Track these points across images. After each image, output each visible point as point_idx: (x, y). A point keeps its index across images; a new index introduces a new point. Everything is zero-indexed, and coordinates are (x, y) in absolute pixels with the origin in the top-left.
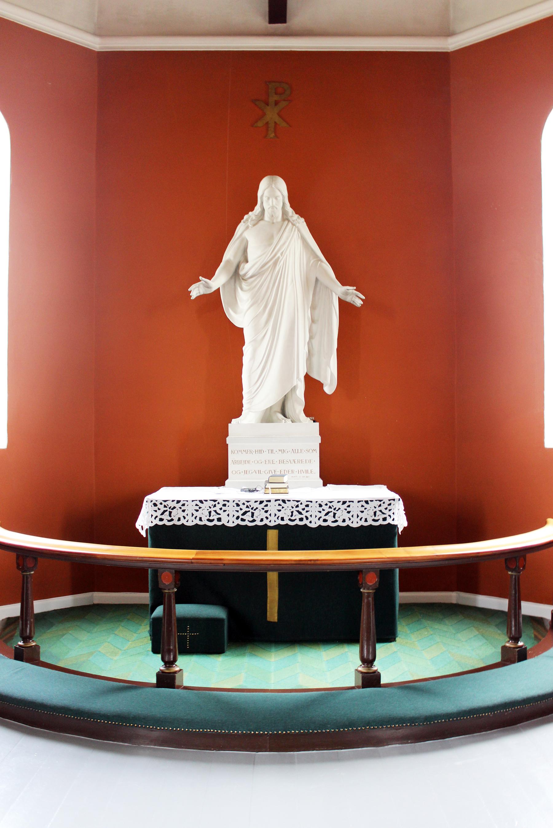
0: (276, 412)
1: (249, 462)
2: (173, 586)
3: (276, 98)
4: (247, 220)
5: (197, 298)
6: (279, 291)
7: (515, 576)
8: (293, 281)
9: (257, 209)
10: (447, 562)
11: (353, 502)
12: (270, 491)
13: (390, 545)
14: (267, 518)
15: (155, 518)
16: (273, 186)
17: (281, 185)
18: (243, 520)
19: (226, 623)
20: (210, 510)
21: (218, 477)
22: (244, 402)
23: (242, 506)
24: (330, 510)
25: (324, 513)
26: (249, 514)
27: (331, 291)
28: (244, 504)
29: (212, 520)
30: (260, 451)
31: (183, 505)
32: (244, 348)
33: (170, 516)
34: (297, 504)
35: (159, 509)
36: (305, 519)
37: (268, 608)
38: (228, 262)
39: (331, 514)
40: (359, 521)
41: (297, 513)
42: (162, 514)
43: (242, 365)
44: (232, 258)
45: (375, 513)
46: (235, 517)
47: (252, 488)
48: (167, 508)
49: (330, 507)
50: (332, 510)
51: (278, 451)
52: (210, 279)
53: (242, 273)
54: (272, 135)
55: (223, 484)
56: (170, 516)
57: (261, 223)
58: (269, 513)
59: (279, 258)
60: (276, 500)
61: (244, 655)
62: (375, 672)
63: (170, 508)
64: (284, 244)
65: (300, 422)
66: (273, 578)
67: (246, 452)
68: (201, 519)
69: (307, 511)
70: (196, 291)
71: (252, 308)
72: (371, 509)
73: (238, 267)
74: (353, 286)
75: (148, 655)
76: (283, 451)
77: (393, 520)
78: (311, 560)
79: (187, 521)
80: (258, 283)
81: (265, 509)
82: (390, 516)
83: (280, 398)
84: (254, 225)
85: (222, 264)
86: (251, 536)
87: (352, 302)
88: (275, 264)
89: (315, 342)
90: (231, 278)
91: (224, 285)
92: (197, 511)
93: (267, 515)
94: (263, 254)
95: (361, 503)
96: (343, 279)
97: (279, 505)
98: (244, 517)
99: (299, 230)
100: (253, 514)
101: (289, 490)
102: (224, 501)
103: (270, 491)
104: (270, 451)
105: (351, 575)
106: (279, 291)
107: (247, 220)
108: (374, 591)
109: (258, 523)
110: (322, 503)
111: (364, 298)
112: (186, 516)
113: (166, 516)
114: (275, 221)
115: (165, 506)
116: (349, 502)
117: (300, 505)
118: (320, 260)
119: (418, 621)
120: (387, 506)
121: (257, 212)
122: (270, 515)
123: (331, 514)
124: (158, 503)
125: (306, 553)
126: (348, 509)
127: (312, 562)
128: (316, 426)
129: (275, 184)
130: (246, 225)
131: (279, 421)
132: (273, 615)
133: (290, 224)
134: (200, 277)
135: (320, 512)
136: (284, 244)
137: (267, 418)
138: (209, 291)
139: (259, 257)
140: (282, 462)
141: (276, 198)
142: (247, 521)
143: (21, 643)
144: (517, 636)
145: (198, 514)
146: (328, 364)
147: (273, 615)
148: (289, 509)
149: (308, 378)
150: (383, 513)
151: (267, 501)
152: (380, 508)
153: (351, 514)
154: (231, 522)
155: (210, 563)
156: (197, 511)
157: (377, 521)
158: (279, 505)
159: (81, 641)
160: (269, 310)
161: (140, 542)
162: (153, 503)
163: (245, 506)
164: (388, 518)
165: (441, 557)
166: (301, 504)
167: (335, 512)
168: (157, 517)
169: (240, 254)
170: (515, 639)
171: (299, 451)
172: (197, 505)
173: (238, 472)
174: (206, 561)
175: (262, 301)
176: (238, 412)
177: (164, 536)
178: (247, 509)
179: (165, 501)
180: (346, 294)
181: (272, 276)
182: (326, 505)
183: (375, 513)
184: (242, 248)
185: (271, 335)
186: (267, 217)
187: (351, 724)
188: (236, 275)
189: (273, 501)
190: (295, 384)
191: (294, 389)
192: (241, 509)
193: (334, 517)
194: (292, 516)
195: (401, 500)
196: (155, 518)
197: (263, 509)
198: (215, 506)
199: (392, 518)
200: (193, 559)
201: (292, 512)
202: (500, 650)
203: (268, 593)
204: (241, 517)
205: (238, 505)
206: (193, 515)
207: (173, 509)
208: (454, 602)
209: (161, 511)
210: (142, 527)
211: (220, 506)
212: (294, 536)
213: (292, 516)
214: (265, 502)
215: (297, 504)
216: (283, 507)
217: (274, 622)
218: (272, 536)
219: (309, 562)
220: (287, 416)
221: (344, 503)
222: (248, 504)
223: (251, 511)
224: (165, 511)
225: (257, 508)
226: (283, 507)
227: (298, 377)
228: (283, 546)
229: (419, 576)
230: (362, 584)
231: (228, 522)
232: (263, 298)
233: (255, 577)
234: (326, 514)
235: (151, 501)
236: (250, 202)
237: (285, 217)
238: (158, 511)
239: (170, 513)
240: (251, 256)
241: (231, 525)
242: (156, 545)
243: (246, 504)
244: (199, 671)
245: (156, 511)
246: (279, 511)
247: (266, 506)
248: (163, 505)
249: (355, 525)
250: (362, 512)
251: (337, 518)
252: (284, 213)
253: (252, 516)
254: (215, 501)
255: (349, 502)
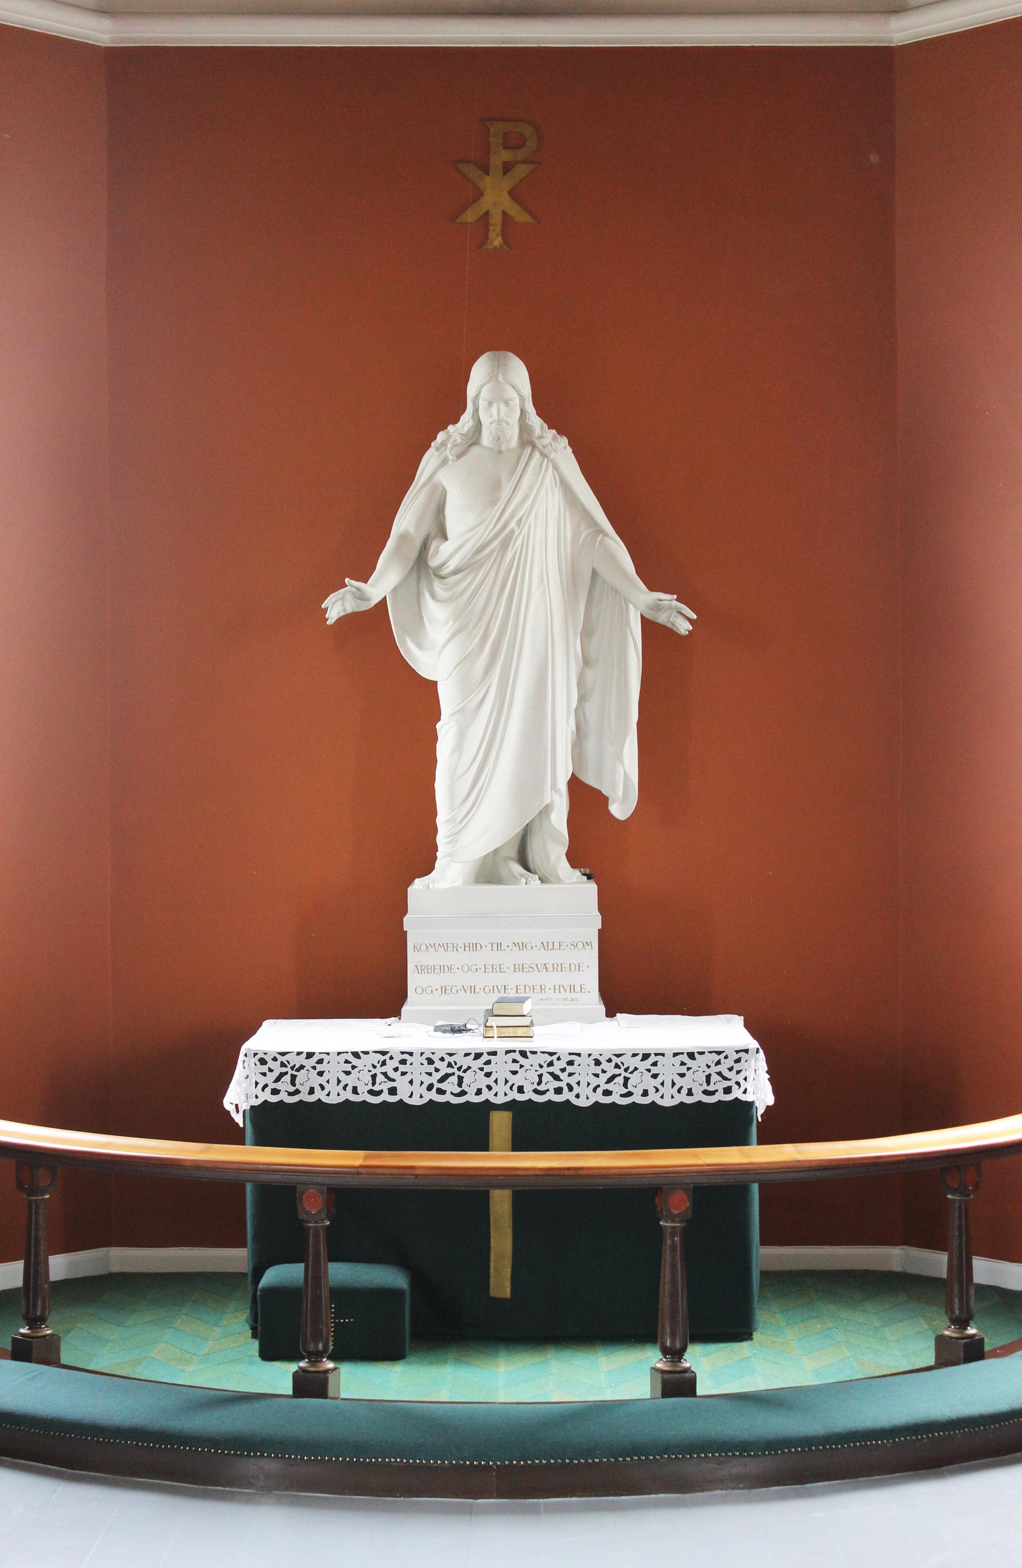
0: (507, 858)
1: (450, 968)
2: (323, 1216)
3: (506, 156)
4: (444, 444)
5: (339, 620)
6: (514, 609)
7: (960, 1201)
8: (542, 580)
9: (466, 420)
10: (818, 1173)
11: (663, 1055)
12: (495, 1032)
13: (742, 1140)
14: (489, 1088)
15: (263, 1089)
16: (500, 378)
17: (518, 374)
18: (441, 1092)
19: (408, 1298)
20: (374, 1071)
21: (386, 998)
22: (440, 839)
23: (438, 1064)
24: (617, 1071)
25: (604, 1077)
26: (454, 1079)
27: (626, 602)
28: (442, 1059)
29: (379, 1093)
30: (475, 947)
31: (320, 1061)
32: (438, 726)
33: (293, 1084)
34: (549, 1059)
35: (271, 1070)
36: (566, 1089)
37: (492, 1270)
38: (404, 537)
39: (620, 1080)
40: (676, 1094)
41: (551, 1078)
42: (277, 1080)
43: (434, 761)
44: (412, 530)
45: (708, 1078)
46: (425, 1086)
47: (458, 1023)
48: (286, 1066)
49: (617, 1066)
50: (621, 1071)
51: (511, 945)
52: (366, 582)
53: (434, 562)
54: (498, 242)
55: (396, 1013)
56: (293, 1084)
57: (475, 451)
58: (493, 1077)
59: (512, 532)
60: (507, 1052)
61: (445, 1362)
62: (687, 1370)
63: (292, 1068)
64: (525, 499)
65: (559, 881)
66: (501, 1204)
67: (445, 947)
68: (355, 1091)
69: (570, 1075)
70: (337, 606)
71: (456, 639)
72: (701, 1070)
73: (425, 546)
74: (672, 594)
75: (252, 1363)
76: (522, 946)
77: (745, 1092)
78: (569, 1169)
79: (328, 1095)
80: (470, 584)
81: (486, 1070)
82: (738, 1083)
83: (517, 829)
84: (459, 456)
85: (390, 544)
86: (460, 1124)
87: (669, 625)
88: (505, 545)
89: (591, 708)
90: (412, 569)
91: (395, 591)
92: (348, 1073)
93: (490, 1082)
94: (480, 524)
95: (680, 1058)
96: (653, 573)
97: (515, 1061)
98: (443, 1086)
99: (556, 468)
100: (460, 1080)
101: (536, 1030)
102: (402, 1053)
103: (495, 1032)
104: (495, 946)
105: (643, 1195)
106: (514, 609)
107: (444, 444)
108: (684, 1225)
109: (472, 1098)
110: (600, 1058)
111: (695, 617)
112: (325, 1084)
113: (285, 1085)
114: (503, 448)
115: (283, 1065)
116: (656, 1055)
117: (555, 1062)
118: (601, 531)
119: (808, 1304)
120: (733, 1064)
121: (466, 429)
122: (496, 1081)
123: (620, 1080)
124: (268, 1058)
125: (554, 1156)
126: (654, 1070)
127: (572, 1172)
128: (593, 887)
129: (504, 375)
130: (443, 456)
131: (513, 880)
132: (501, 1282)
133: (537, 455)
134: (347, 580)
135: (597, 1075)
136: (525, 499)
137: (488, 873)
138: (364, 607)
139: (471, 530)
140: (519, 968)
141: (506, 403)
142: (448, 1093)
143: (24, 1331)
144: (964, 1316)
145: (350, 1081)
146: (619, 757)
147: (501, 1282)
148: (533, 1069)
149: (575, 785)
150: (725, 1079)
151: (489, 1054)
152: (718, 1068)
153: (660, 1079)
154: (416, 1096)
155: (391, 1174)
156: (348, 1073)
157: (713, 1093)
158: (515, 1061)
159: (108, 1341)
160: (491, 643)
161: (233, 1135)
162: (258, 1057)
163: (446, 1063)
164: (735, 1087)
165: (806, 1164)
166: (559, 1059)
167: (627, 1075)
168: (266, 1086)
169: (429, 518)
170: (962, 1323)
171: (556, 946)
172: (347, 1062)
173: (429, 990)
174: (383, 1171)
175: (475, 627)
176: (427, 867)
177: (275, 1123)
178: (450, 1070)
179: (283, 1054)
180: (657, 607)
181: (499, 568)
182: (610, 1061)
183: (708, 1078)
184: (433, 506)
185: (496, 694)
186: (486, 439)
187: (637, 1450)
188: (420, 565)
189: (501, 1054)
190: (547, 802)
191: (546, 811)
192: (437, 1070)
193: (625, 1085)
194: (539, 1083)
195: (761, 1051)
196: (263, 1089)
197: (482, 1069)
198: (384, 1063)
199: (742, 1089)
200: (361, 1167)
201: (540, 1076)
202: (933, 1342)
203: (492, 1239)
204: (437, 1085)
205: (430, 1061)
206: (339, 1082)
207: (298, 1070)
208: (897, 1268)
209: (276, 1074)
210: (237, 1106)
211: (395, 1063)
212: (542, 1123)
213: (539, 1083)
214: (485, 1054)
215: (549, 1059)
216: (521, 1066)
217: (505, 1300)
218: (500, 1124)
219: (566, 1173)
220: (532, 867)
221: (646, 1057)
222: (451, 1059)
223: (457, 1073)
224: (282, 1075)
225: (469, 1068)
226: (521, 1066)
227: (554, 787)
228: (520, 1143)
229: (810, 1205)
230: (661, 1212)
231: (411, 1096)
232: (479, 620)
233: (468, 1198)
234: (610, 1080)
235: (255, 1054)
236: (453, 405)
237: (526, 437)
238: (268, 1074)
239: (293, 1078)
240: (453, 526)
241: (416, 1101)
242: (262, 1140)
243: (448, 1059)
244: (360, 1382)
245: (264, 1074)
246: (514, 1073)
247: (488, 1062)
248: (278, 1063)
249: (667, 1103)
250: (682, 1075)
251: (630, 1088)
252: (524, 428)
253: (460, 1084)
254: (384, 1053)
255: (656, 1055)
